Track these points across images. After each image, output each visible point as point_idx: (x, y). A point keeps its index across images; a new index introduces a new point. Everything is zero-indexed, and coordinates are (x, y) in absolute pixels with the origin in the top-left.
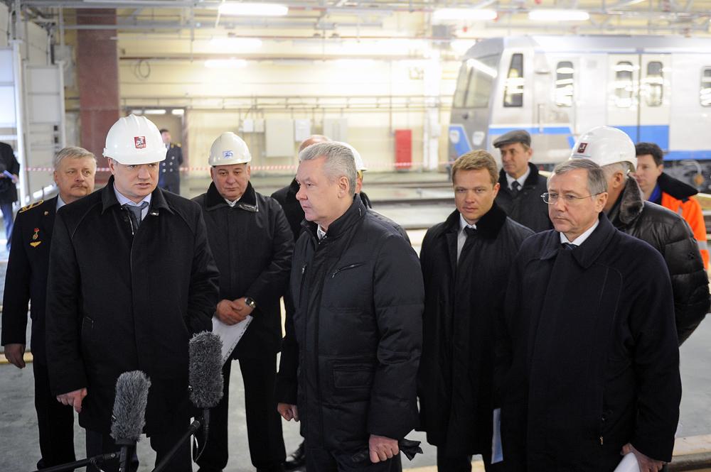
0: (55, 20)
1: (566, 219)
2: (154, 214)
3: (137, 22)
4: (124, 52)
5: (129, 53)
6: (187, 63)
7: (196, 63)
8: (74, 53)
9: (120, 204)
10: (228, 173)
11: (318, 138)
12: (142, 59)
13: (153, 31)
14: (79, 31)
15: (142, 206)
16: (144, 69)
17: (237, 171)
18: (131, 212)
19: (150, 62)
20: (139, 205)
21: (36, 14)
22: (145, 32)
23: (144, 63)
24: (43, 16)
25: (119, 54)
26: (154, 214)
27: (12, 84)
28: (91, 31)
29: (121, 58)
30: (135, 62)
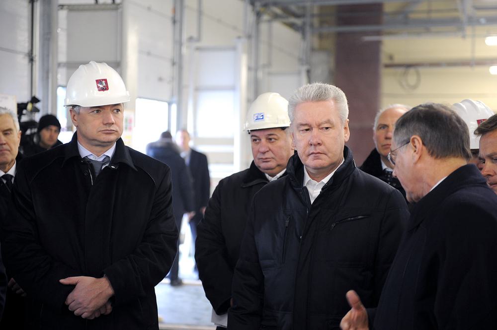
0: (308, 20)
1: (273, 158)
2: (113, 167)
3: (406, 21)
4: (391, 57)
5: (398, 59)
6: (466, 70)
7: (478, 69)
8: (332, 60)
9: (80, 156)
10: (260, 140)
11: (402, 108)
12: (409, 66)
13: (428, 31)
14: (339, 34)
15: (103, 161)
16: (412, 78)
17: (270, 137)
18: (92, 165)
19: (421, 70)
20: (101, 159)
21: (291, 16)
22: (419, 34)
23: (412, 71)
24: (297, 16)
25: (384, 60)
26: (113, 167)
27: (233, 88)
28: (354, 33)
29: (387, 66)
30: (400, 70)
